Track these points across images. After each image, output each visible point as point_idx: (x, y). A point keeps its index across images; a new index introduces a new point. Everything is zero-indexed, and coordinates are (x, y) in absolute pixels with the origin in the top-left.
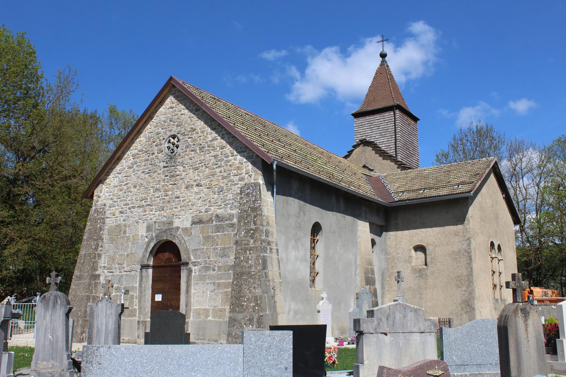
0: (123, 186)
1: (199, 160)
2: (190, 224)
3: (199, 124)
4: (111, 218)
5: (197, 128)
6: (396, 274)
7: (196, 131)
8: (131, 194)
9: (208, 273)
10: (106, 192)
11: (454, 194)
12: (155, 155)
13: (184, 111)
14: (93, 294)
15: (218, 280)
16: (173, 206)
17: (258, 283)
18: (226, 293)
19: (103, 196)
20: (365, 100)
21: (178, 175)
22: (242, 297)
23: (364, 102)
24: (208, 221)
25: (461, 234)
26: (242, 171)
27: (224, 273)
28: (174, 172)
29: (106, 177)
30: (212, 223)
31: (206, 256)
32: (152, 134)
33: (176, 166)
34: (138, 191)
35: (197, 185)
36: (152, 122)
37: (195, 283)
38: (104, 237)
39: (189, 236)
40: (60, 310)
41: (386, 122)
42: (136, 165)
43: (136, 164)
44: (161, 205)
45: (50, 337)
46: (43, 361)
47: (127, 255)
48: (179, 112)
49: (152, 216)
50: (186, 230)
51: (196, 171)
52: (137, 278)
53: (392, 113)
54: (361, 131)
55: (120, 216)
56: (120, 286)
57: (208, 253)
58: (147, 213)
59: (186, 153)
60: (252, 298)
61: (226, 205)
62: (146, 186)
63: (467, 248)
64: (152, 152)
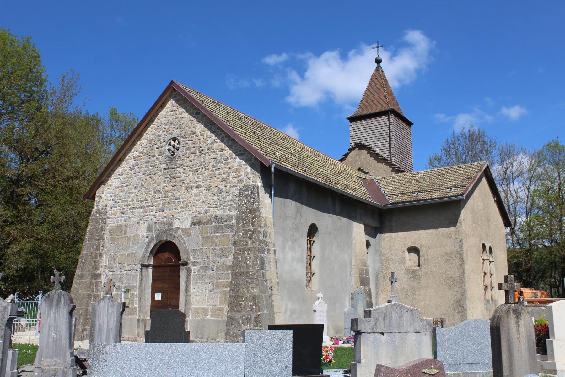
0: (124, 187)
2: (190, 224)
3: (199, 127)
4: (112, 218)
5: (197, 131)
8: (132, 195)
9: (207, 273)
11: (447, 197)
12: (156, 157)
13: (185, 114)
14: (94, 293)
15: (217, 280)
16: (173, 207)
17: (256, 283)
19: (105, 196)
20: (360, 104)
21: (178, 177)
22: (240, 296)
23: (359, 106)
24: (207, 222)
25: (453, 236)
26: (241, 174)
27: (223, 272)
29: (108, 178)
30: (211, 224)
31: (205, 256)
32: (153, 136)
33: (177, 168)
34: (139, 193)
35: (197, 187)
39: (189, 237)
40: (64, 308)
41: (380, 126)
42: (137, 167)
43: (137, 165)
44: (161, 206)
45: (54, 335)
46: (47, 357)
47: (128, 255)
49: (153, 217)
50: (185, 230)
51: (196, 173)
52: (137, 277)
53: (387, 118)
54: (356, 135)
55: (121, 216)
56: (120, 285)
58: (147, 213)
60: (250, 298)
61: (225, 206)
62: (146, 188)
64: (153, 154)
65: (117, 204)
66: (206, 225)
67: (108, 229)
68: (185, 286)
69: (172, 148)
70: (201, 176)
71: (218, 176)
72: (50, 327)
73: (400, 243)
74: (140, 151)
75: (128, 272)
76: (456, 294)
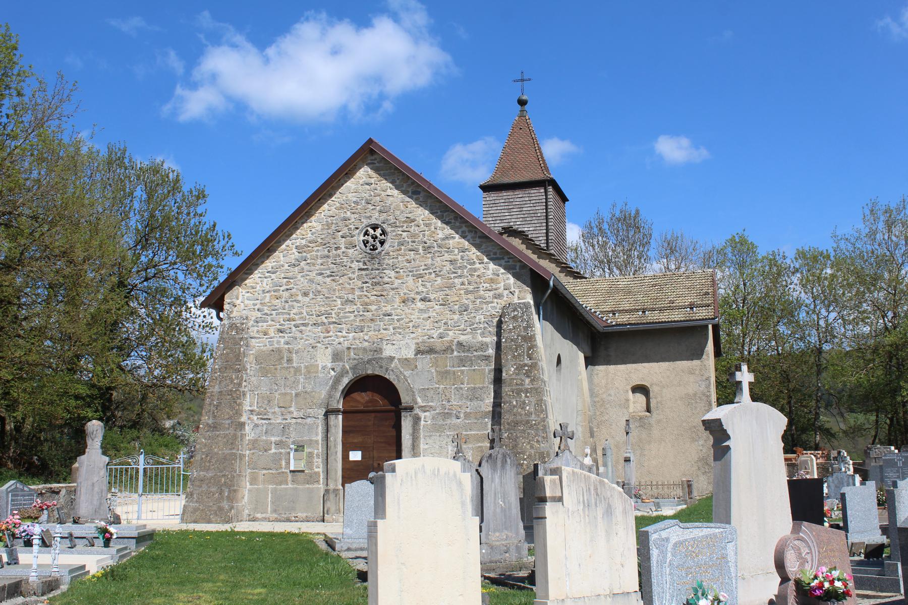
0: (281, 292)
1: (423, 264)
2: (414, 353)
3: (420, 212)
4: (260, 338)
5: (417, 219)
6: (625, 422)
7: (416, 222)
8: (299, 305)
9: (448, 421)
10: (248, 299)
11: (694, 320)
12: (341, 251)
13: (392, 191)
14: (240, 452)
17: (543, 435)
18: (479, 449)
19: (242, 304)
20: (497, 166)
22: (520, 453)
23: (496, 169)
25: (697, 372)
26: (498, 286)
28: (378, 278)
29: (246, 276)
32: (332, 218)
33: (383, 270)
35: (422, 300)
36: (332, 201)
37: (426, 435)
38: (249, 367)
40: (511, 471)
41: (532, 202)
42: (304, 262)
43: (305, 260)
44: (357, 324)
45: (501, 503)
46: (495, 531)
47: (297, 395)
48: (382, 192)
49: (342, 339)
50: (406, 361)
51: (420, 280)
52: (317, 428)
53: (542, 191)
54: (493, 212)
55: (277, 335)
56: (284, 439)
57: (447, 394)
58: (331, 333)
59: (400, 252)
60: (535, 455)
61: (475, 329)
63: (706, 391)
64: (336, 246)
65: (269, 318)
66: (443, 354)
67: (253, 354)
68: (410, 442)
69: (371, 240)
70: (428, 285)
71: (459, 286)
72: (495, 494)
73: (621, 379)
74: (308, 238)
75: (299, 421)
76: (701, 448)
